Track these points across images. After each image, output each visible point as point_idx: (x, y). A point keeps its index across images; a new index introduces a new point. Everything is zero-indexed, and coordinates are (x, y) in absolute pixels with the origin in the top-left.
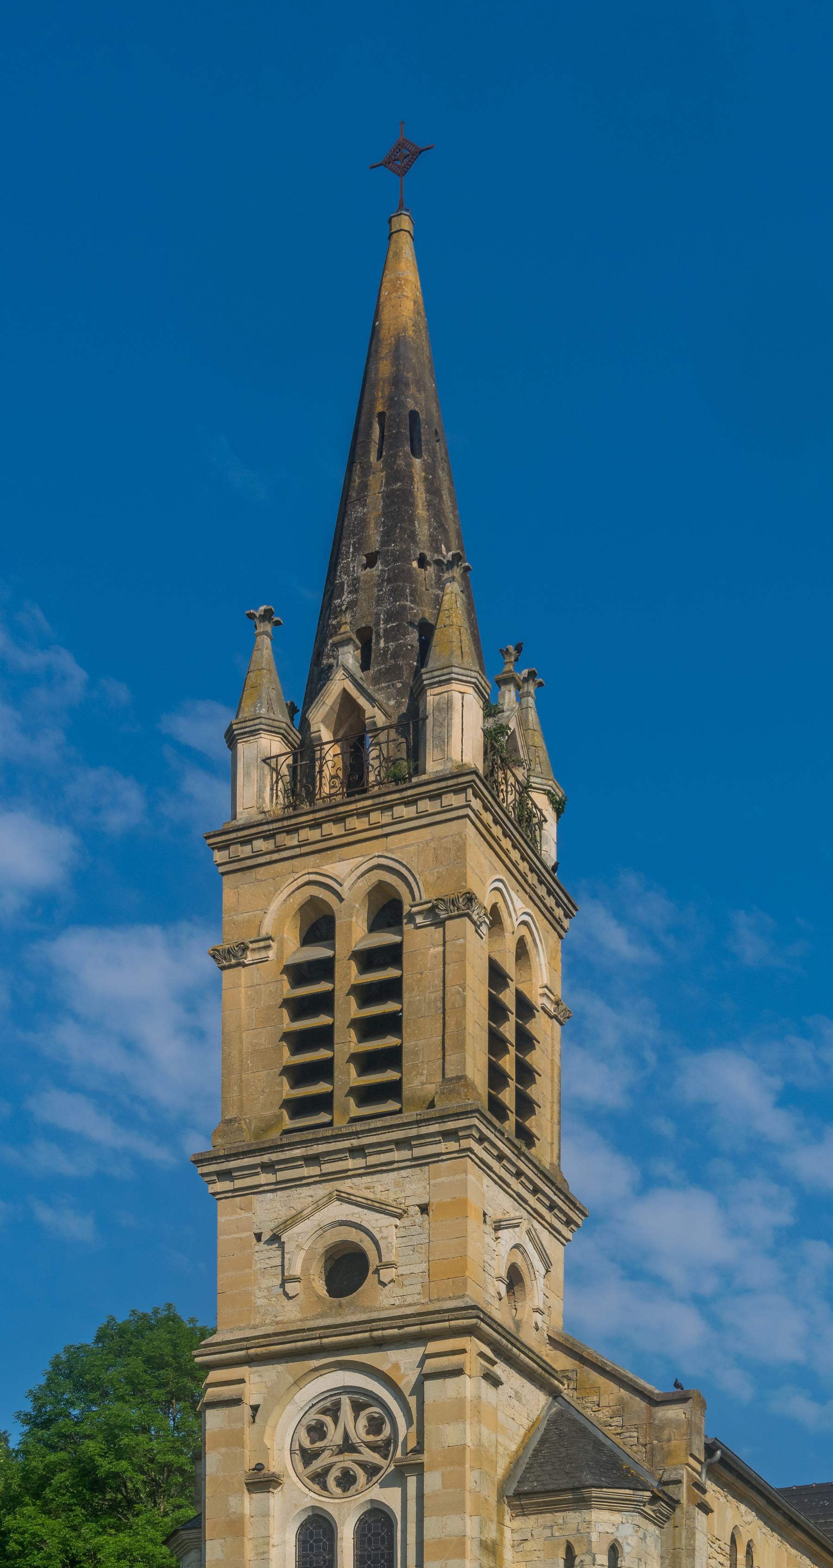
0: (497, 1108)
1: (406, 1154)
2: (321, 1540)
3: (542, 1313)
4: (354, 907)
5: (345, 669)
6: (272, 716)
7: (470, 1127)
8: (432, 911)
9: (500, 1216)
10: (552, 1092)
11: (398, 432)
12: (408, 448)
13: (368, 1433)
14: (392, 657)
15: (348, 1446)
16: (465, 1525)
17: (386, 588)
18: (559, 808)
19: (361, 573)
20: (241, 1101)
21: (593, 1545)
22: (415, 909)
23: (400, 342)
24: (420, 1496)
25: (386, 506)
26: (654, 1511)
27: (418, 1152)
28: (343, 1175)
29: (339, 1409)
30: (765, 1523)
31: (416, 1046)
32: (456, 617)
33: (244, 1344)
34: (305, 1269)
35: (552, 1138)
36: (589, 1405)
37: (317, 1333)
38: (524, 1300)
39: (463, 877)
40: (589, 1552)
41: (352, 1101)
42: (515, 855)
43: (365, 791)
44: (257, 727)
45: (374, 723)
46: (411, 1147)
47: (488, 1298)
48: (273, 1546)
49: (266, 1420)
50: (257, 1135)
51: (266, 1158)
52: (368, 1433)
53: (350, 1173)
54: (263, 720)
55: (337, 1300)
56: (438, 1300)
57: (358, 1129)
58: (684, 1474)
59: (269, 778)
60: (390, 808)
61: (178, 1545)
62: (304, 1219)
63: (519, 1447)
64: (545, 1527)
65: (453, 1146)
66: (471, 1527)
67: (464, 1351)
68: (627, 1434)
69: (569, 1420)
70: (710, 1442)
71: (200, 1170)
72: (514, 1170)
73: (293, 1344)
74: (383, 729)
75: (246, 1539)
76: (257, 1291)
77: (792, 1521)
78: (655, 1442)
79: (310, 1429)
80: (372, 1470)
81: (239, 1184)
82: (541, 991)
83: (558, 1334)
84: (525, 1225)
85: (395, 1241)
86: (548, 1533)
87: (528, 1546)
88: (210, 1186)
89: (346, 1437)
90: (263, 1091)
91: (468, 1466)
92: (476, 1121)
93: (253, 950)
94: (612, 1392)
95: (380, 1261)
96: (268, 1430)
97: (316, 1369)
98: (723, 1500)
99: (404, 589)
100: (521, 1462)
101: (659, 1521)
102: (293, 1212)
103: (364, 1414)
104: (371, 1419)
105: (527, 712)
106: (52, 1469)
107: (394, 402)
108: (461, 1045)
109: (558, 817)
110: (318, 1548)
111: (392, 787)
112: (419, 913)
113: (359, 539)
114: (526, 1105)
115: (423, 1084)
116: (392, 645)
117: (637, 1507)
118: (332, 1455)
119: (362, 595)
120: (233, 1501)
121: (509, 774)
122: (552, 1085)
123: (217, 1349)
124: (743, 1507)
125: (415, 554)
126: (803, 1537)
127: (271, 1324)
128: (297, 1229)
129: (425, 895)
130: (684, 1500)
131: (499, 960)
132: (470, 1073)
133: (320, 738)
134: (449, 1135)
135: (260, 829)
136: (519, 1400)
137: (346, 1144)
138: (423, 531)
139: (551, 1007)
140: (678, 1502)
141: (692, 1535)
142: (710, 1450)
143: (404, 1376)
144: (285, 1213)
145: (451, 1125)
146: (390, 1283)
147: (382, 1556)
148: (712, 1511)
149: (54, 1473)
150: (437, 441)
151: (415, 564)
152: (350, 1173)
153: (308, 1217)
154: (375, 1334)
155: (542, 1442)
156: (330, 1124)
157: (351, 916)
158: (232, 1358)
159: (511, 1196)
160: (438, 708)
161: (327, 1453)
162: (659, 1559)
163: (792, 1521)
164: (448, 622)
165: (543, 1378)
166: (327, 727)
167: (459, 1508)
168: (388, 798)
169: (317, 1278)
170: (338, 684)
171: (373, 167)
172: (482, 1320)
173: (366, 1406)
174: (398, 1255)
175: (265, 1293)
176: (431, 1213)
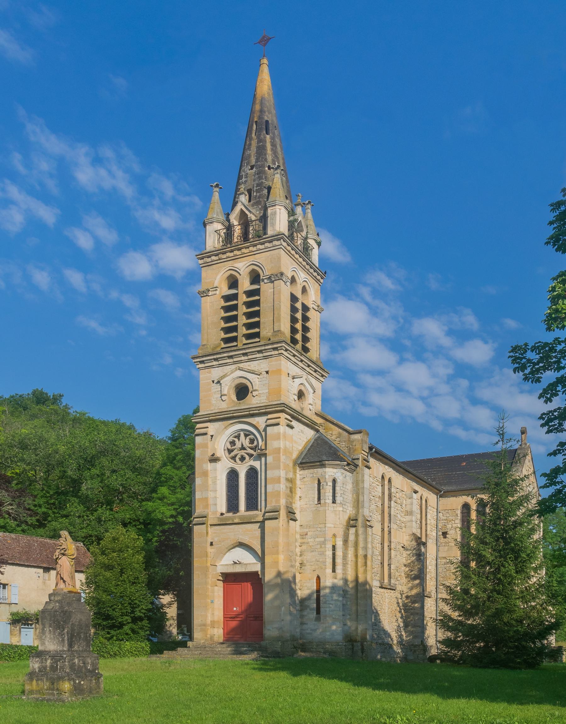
0: (294, 341)
1: (261, 355)
3: (312, 405)
6: (218, 217)
7: (282, 346)
8: (269, 278)
11: (262, 127)
12: (265, 132)
13: (250, 444)
15: (243, 448)
17: (257, 176)
19: (248, 171)
22: (264, 278)
23: (262, 99)
24: (266, 464)
25: (257, 151)
27: (265, 354)
28: (240, 362)
33: (208, 416)
34: (228, 392)
37: (232, 412)
39: (280, 267)
40: (325, 481)
41: (244, 338)
43: (249, 240)
45: (251, 219)
46: (263, 353)
47: (290, 401)
49: (215, 440)
50: (213, 349)
51: (215, 357)
52: (250, 444)
62: (228, 376)
63: (303, 448)
65: (276, 352)
66: (282, 474)
67: (280, 418)
71: (194, 361)
72: (300, 360)
74: (254, 221)
77: (407, 471)
79: (231, 443)
80: (251, 456)
81: (207, 365)
82: (312, 303)
83: (318, 412)
84: (305, 377)
86: (312, 475)
89: (242, 445)
91: (281, 454)
92: (284, 345)
94: (336, 430)
96: (216, 443)
97: (232, 424)
98: (378, 464)
101: (351, 471)
102: (224, 374)
103: (248, 438)
104: (250, 439)
106: (176, 455)
107: (260, 118)
108: (279, 320)
109: (319, 247)
111: (257, 239)
112: (265, 279)
114: (306, 339)
116: (258, 194)
117: (342, 467)
119: (249, 179)
120: (204, 466)
121: (299, 234)
123: (202, 417)
124: (387, 467)
126: (411, 476)
127: (217, 409)
128: (225, 379)
129: (267, 273)
130: (360, 464)
131: (295, 294)
133: (233, 224)
134: (275, 349)
136: (303, 433)
138: (269, 158)
139: (316, 308)
140: (358, 465)
141: (363, 476)
142: (371, 448)
143: (261, 425)
144: (222, 374)
145: (275, 346)
147: (254, 483)
149: (177, 456)
151: (267, 169)
153: (229, 375)
154: (251, 412)
155: (311, 446)
156: (237, 346)
160: (272, 214)
162: (352, 484)
163: (407, 471)
164: (275, 187)
166: (236, 220)
167: (279, 468)
168: (255, 243)
169: (232, 395)
170: (239, 207)
171: (255, 44)
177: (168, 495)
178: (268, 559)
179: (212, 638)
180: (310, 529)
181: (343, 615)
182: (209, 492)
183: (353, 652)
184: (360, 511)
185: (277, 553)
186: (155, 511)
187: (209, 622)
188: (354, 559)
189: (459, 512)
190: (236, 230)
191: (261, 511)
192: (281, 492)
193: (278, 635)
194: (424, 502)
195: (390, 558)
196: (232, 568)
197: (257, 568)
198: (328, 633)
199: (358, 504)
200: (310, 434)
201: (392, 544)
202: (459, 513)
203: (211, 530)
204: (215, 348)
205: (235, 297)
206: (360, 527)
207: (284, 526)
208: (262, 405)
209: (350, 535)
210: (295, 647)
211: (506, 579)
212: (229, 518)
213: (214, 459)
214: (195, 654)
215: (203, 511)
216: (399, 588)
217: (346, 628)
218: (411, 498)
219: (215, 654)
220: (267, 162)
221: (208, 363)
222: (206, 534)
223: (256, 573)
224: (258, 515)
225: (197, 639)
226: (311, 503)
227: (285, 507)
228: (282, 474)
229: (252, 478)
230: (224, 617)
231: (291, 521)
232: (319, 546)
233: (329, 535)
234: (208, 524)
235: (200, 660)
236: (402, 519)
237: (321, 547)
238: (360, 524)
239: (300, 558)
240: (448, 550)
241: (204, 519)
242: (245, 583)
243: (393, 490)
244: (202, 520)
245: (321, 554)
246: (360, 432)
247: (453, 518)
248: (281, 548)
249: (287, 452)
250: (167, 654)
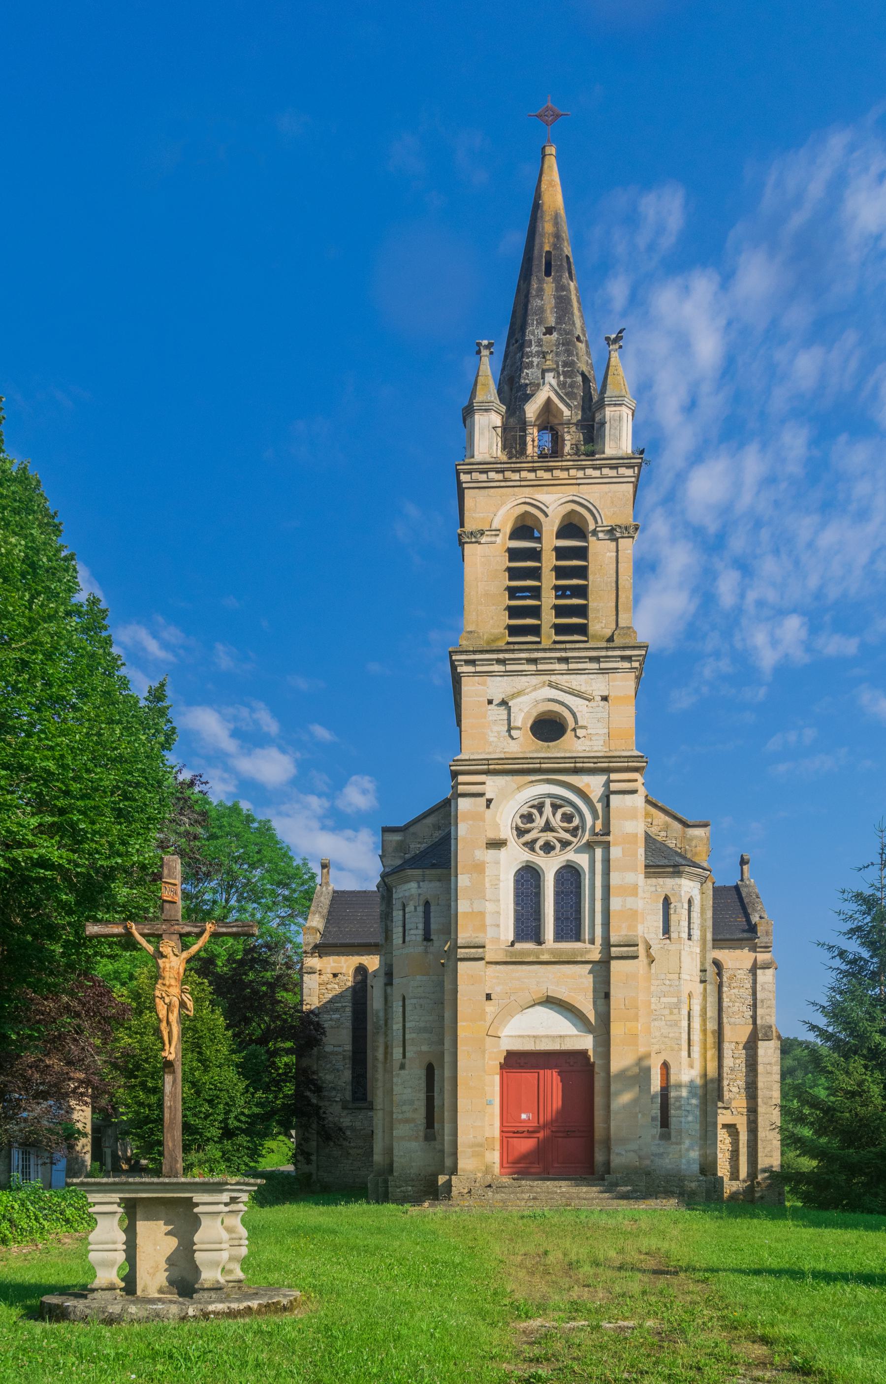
5: (551, 385)
8: (611, 531)
15: (548, 828)
17: (561, 348)
25: (556, 303)
27: (603, 665)
28: (551, 672)
29: (543, 806)
50: (488, 643)
51: (501, 656)
55: (546, 744)
76: (490, 733)
86: (653, 889)
97: (532, 782)
102: (515, 690)
112: (602, 531)
113: (540, 318)
135: (495, 466)
137: (558, 655)
144: (510, 690)
156: (539, 643)
161: (536, 831)
173: (561, 806)
175: (496, 734)
191: (592, 942)
197: (586, 1043)
204: (494, 641)
208: (592, 754)
213: (497, 844)
215: (474, 935)
221: (483, 665)
225: (464, 1170)
230: (502, 1132)
232: (667, 1012)
237: (671, 1013)
241: (481, 950)
244: (477, 952)
245: (671, 1026)
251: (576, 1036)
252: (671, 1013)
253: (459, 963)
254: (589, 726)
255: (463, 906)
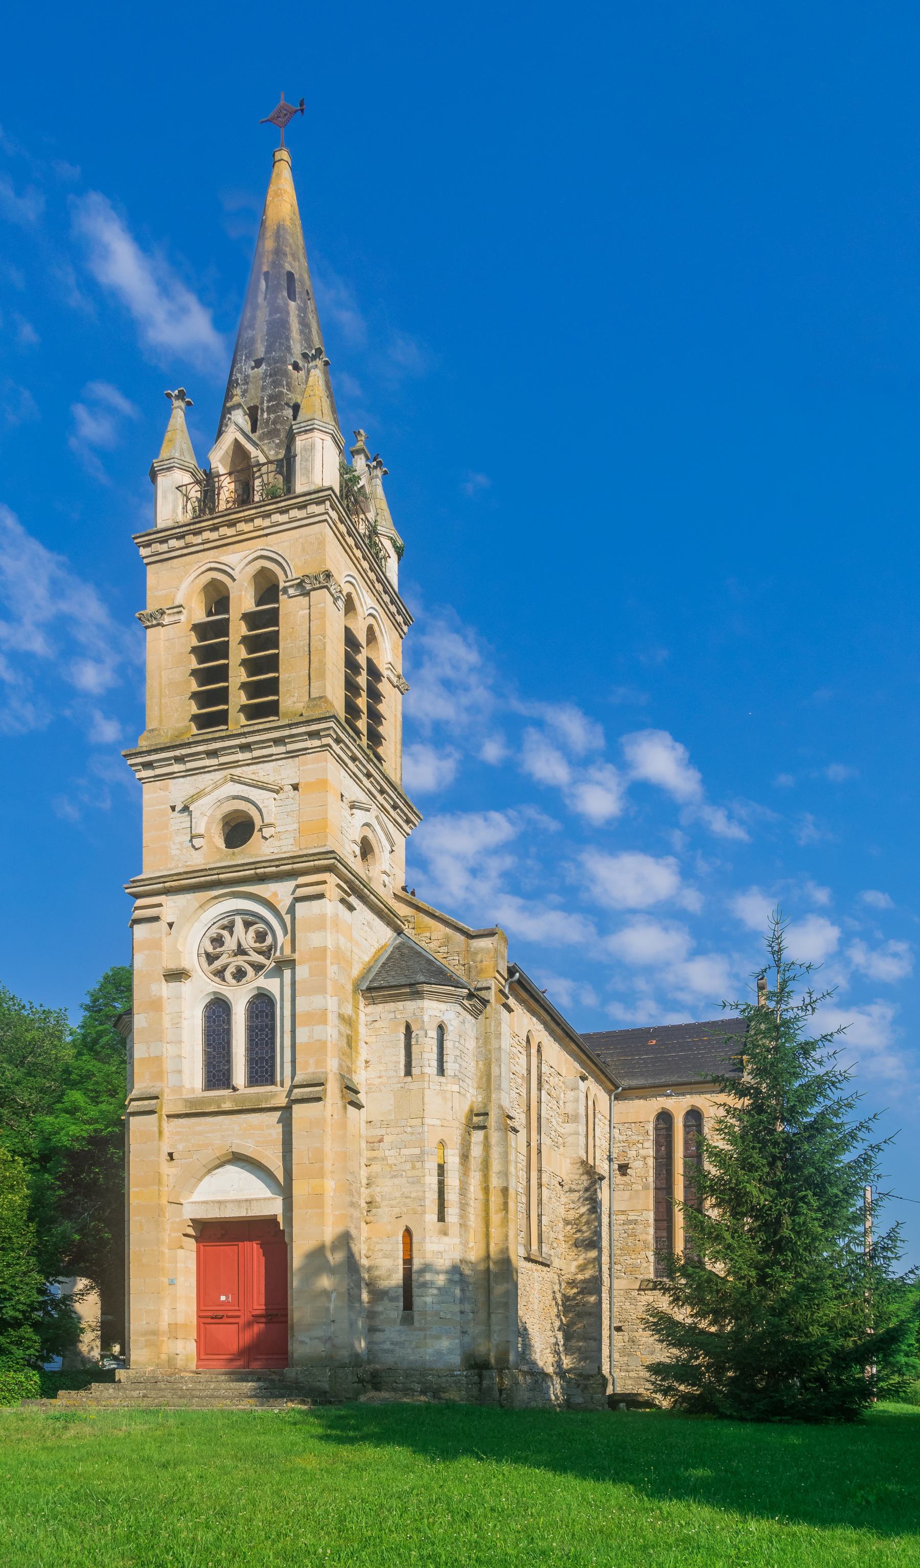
1: (282, 749)
2: (222, 1016)
4: (243, 585)
5: (236, 425)
6: (183, 459)
7: (328, 729)
8: (300, 585)
9: (353, 799)
10: (396, 735)
12: (285, 294)
13: (255, 942)
14: (272, 424)
16: (326, 1001)
17: (268, 380)
18: (400, 552)
19: (250, 371)
20: (161, 717)
21: (425, 1024)
22: (288, 584)
24: (293, 983)
26: (470, 1005)
27: (290, 747)
28: (235, 764)
30: (550, 1034)
31: (289, 677)
32: (318, 390)
33: (162, 880)
34: (208, 829)
35: (396, 765)
36: (423, 939)
37: (215, 872)
38: (375, 864)
40: (422, 1028)
41: (242, 716)
42: (365, 565)
44: (172, 465)
45: (258, 461)
46: (285, 744)
48: (185, 1019)
51: (178, 753)
52: (255, 942)
53: (240, 763)
54: (176, 460)
56: (306, 848)
57: (246, 731)
58: (492, 984)
59: (181, 500)
60: (269, 516)
61: (124, 1027)
62: (206, 795)
64: (390, 1012)
65: (316, 743)
66: (332, 1004)
67: (325, 882)
68: (451, 958)
69: (409, 947)
70: (511, 965)
71: (129, 762)
73: (198, 879)
75: (164, 1014)
78: (471, 963)
80: (258, 968)
85: (274, 809)
86: (392, 1015)
87: (376, 1025)
88: (137, 774)
89: (239, 945)
90: (177, 711)
91: (328, 961)
92: (332, 724)
93: (169, 614)
94: (440, 930)
95: (263, 822)
97: (215, 898)
99: (281, 381)
100: (372, 970)
101: (476, 1013)
102: (198, 790)
105: (376, 489)
106: (100, 1035)
107: (276, 264)
108: (322, 675)
109: (399, 559)
110: (219, 1021)
112: (291, 586)
115: (295, 703)
116: (272, 416)
117: (458, 1000)
118: (229, 957)
119: (251, 386)
120: (154, 987)
122: (396, 732)
124: (534, 1019)
125: (290, 361)
126: (574, 1046)
128: (201, 802)
129: (295, 573)
130: (493, 1000)
132: (329, 695)
136: (371, 928)
139: (395, 680)
140: (488, 1001)
142: (511, 971)
144: (193, 792)
146: (270, 837)
147: (267, 1026)
148: (513, 1011)
150: (309, 299)
151: (290, 367)
152: (240, 763)
153: (209, 793)
154: (258, 871)
155: (388, 959)
157: (241, 591)
158: (153, 890)
159: (363, 790)
160: (305, 449)
164: (312, 393)
165: (389, 916)
166: (224, 466)
167: (323, 991)
169: (217, 836)
170: (230, 435)
172: (338, 861)
174: (275, 819)
175: (178, 846)
176: (300, 789)
177: (83, 1104)
178: (299, 1189)
179: (171, 1361)
180: (389, 1130)
181: (462, 1312)
182: (165, 1045)
183: (480, 1390)
184: (494, 1096)
185: (321, 1175)
186: (59, 1134)
187: (164, 1326)
188: (481, 1196)
189: (651, 1127)
190: (225, 483)
191: (282, 1086)
192: (329, 1044)
193: (324, 1354)
194: (590, 1103)
195: (540, 1202)
196: (217, 1210)
197: (274, 1207)
198: (430, 1351)
199: (487, 1082)
200: (384, 935)
201: (544, 1175)
202: (651, 1128)
203: (169, 1127)
205: (222, 628)
206: (493, 1129)
207: (335, 1117)
209: (472, 1144)
210: (361, 1381)
211: (800, 1239)
212: (211, 1101)
213: (176, 975)
214: (132, 1397)
216: (557, 1263)
217: (467, 1339)
218: (575, 1088)
219: (180, 1397)
220: (291, 354)
221: (161, 766)
222: (157, 1135)
223: (272, 1221)
224: (278, 1094)
226: (392, 1073)
227: (338, 1077)
228: (332, 1004)
229: (262, 1016)
230: (199, 1317)
231: (350, 1108)
232: (408, 1166)
233: (431, 1143)
234: (163, 1113)
235: (146, 1411)
236: (559, 1129)
237: (414, 1168)
238: (493, 1124)
239: (367, 1191)
240: (630, 1198)
241: (154, 1102)
242: (247, 1244)
243: (545, 1068)
245: (413, 1183)
246: (492, 934)
247: (640, 1138)
248: (328, 1165)
249: (341, 958)
250: (65, 1399)
251: (269, 1199)
252: (414, 1168)
253: (131, 1118)
254: (277, 823)
255: (140, 1051)
